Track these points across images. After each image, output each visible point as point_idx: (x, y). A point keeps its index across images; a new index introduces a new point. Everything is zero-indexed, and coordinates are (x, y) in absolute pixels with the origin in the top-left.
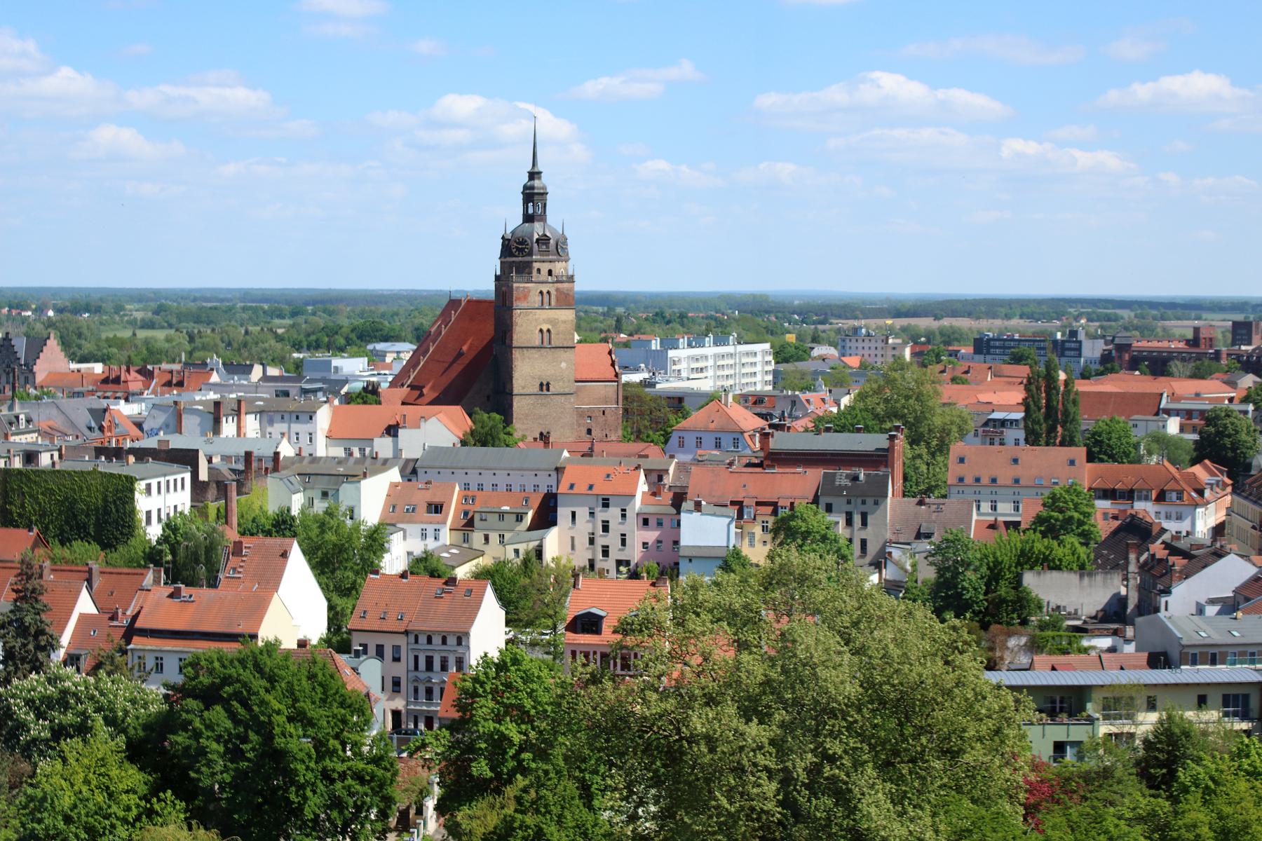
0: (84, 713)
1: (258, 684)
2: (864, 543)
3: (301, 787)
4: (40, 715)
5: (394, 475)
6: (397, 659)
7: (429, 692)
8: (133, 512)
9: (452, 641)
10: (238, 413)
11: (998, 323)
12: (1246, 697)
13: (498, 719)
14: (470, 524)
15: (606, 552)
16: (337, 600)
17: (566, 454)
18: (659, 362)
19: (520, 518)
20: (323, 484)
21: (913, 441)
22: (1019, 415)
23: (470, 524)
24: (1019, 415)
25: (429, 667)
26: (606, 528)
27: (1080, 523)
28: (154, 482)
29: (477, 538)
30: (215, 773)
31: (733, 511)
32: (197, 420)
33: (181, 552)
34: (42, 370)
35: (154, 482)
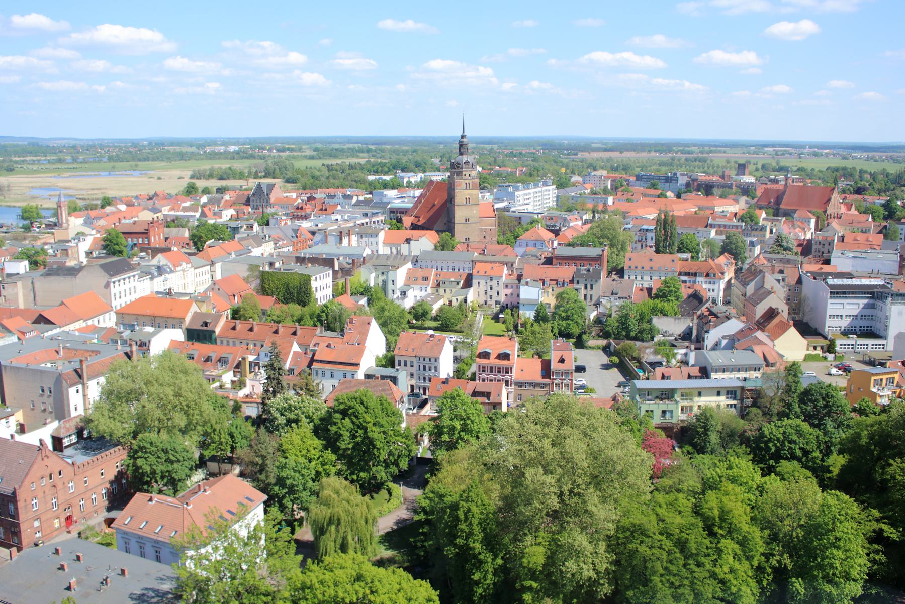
0: (297, 414)
1: (361, 409)
2: (591, 296)
3: (378, 449)
4: (282, 414)
5: (409, 265)
6: (412, 366)
7: (424, 379)
8: (311, 288)
9: (433, 360)
10: (349, 234)
11: (644, 154)
12: (735, 392)
13: (452, 419)
14: (439, 285)
15: (491, 298)
16: (389, 337)
17: (476, 254)
18: (512, 197)
19: (458, 283)
20: (382, 269)
21: (612, 246)
22: (653, 227)
23: (439, 285)
24: (653, 227)
25: (424, 369)
26: (491, 289)
27: (676, 292)
28: (318, 276)
29: (441, 291)
30: (345, 443)
31: (541, 283)
32: (333, 238)
33: (330, 317)
34: (273, 198)
35: (318, 276)
